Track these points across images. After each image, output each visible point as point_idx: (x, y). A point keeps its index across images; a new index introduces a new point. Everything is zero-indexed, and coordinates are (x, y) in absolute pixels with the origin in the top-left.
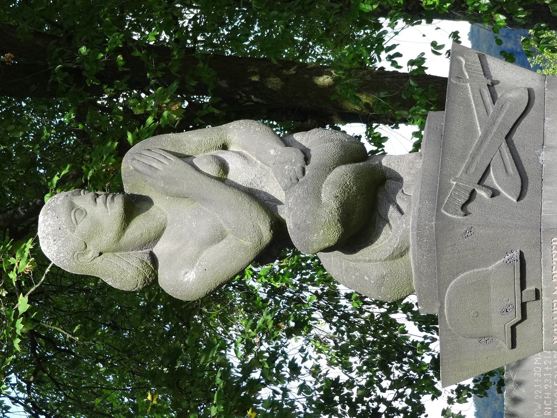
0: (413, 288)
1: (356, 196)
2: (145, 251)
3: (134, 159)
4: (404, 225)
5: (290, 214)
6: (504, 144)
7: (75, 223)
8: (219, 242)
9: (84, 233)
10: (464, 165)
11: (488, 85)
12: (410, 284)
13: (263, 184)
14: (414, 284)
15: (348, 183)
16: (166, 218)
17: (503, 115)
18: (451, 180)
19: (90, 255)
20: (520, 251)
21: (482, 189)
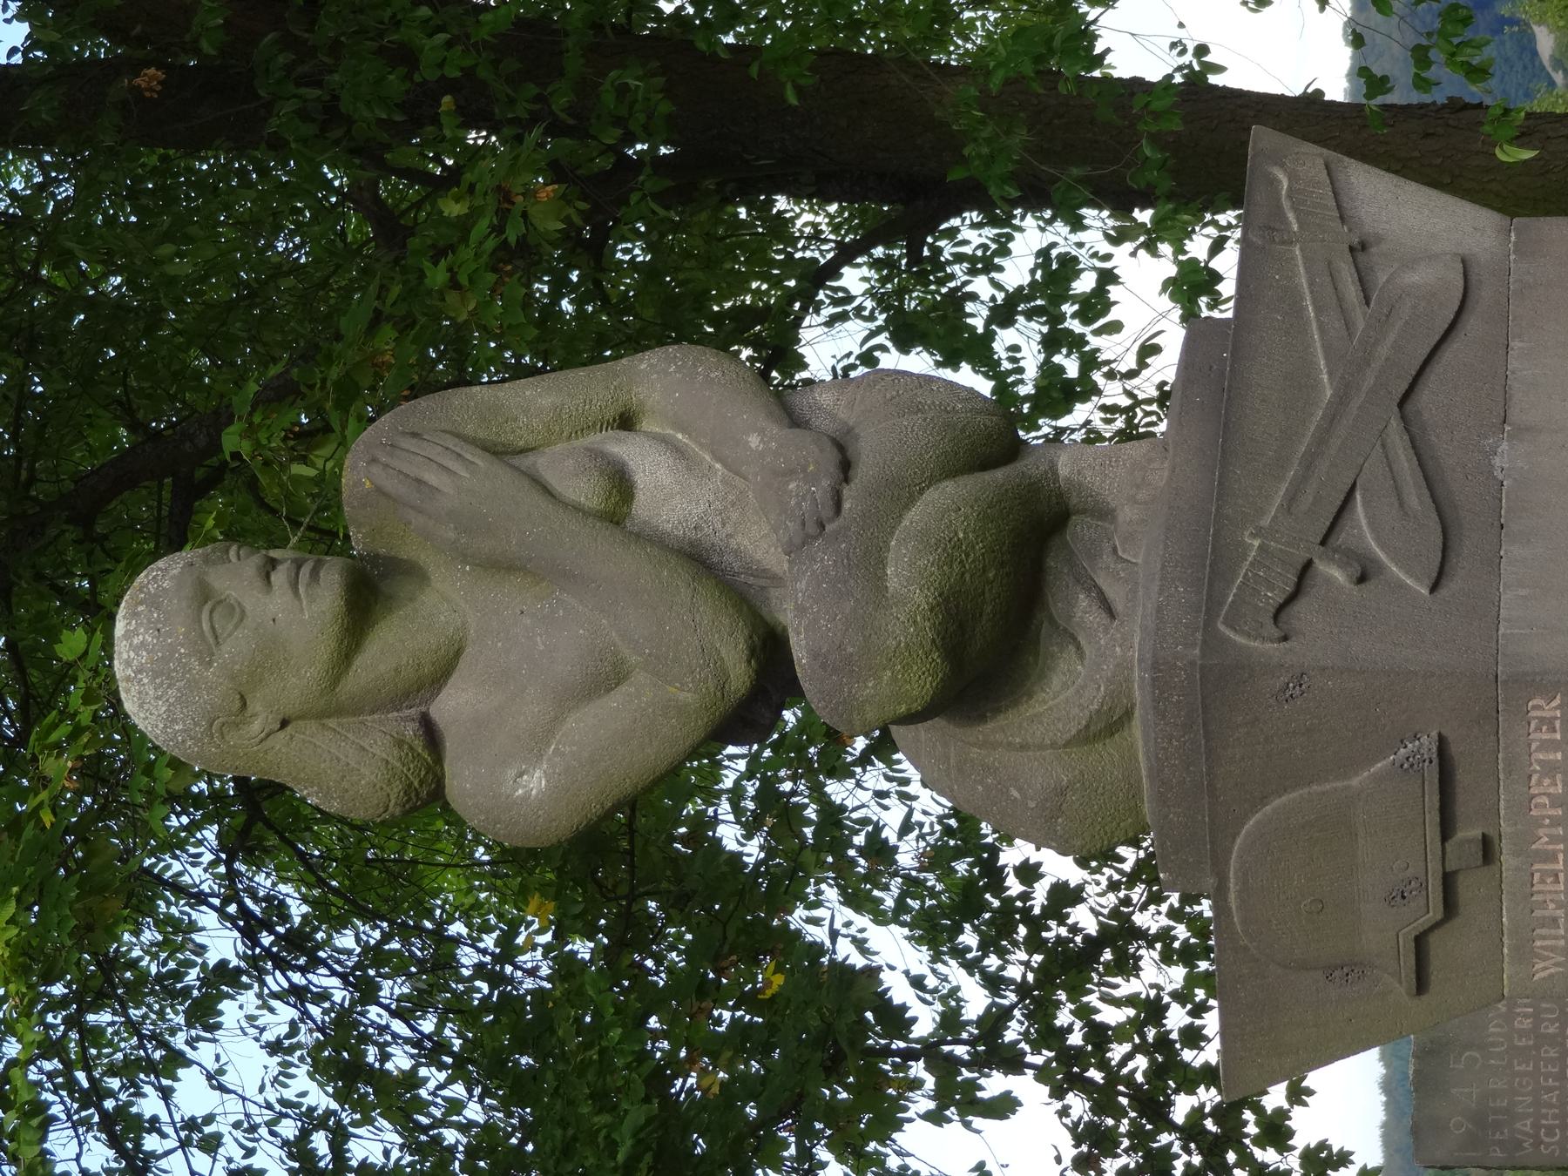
0: (1144, 819)
1: (984, 570)
2: (407, 712)
3: (374, 460)
4: (1118, 649)
5: (800, 623)
6: (1395, 424)
7: (211, 640)
8: (609, 690)
9: (237, 667)
10: (1284, 487)
11: (1352, 249)
12: (1136, 811)
13: (729, 529)
14: (1146, 808)
15: (961, 535)
16: (463, 624)
17: (1392, 337)
18: (1247, 533)
19: (256, 726)
20: (1440, 735)
21: (1333, 560)
